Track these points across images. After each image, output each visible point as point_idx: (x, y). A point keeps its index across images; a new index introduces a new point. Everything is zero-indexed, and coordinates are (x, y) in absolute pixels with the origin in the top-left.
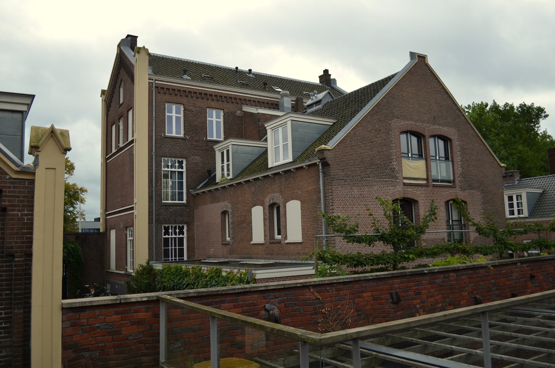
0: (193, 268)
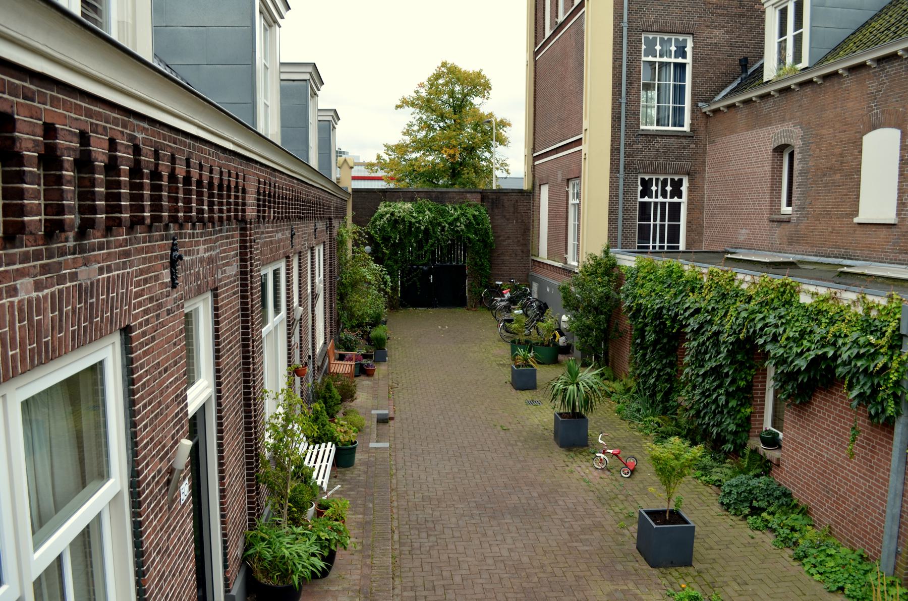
0: (711, 273)
